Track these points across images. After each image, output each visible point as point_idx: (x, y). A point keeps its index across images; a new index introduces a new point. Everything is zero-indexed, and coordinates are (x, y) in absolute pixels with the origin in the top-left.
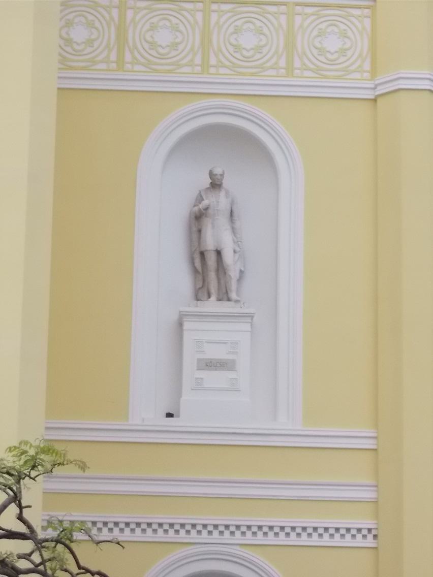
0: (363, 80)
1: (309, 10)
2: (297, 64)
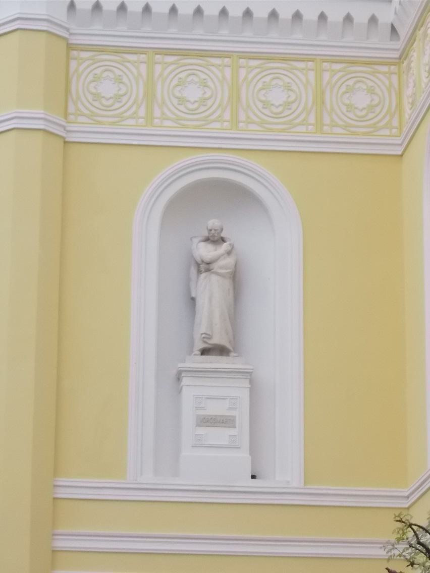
0: (308, 133)
1: (337, 67)
2: (157, 113)
